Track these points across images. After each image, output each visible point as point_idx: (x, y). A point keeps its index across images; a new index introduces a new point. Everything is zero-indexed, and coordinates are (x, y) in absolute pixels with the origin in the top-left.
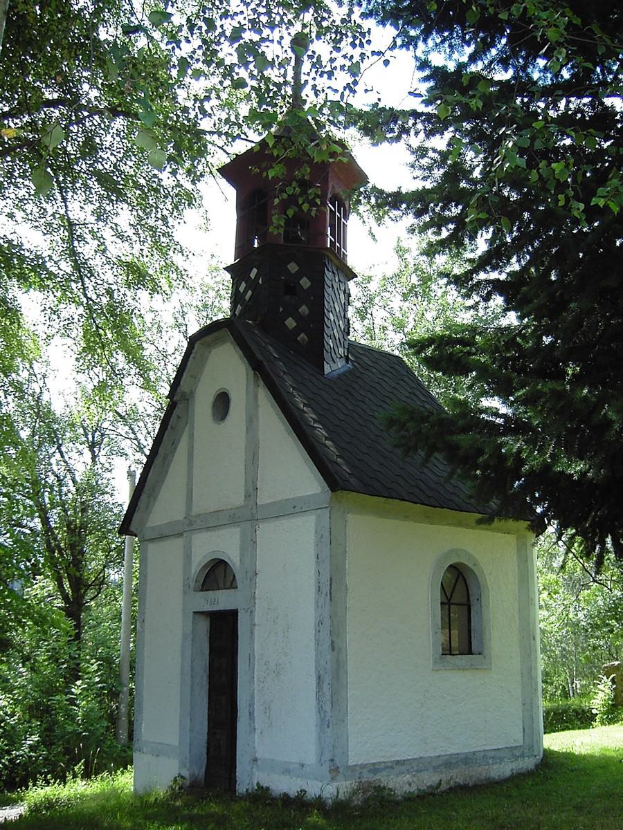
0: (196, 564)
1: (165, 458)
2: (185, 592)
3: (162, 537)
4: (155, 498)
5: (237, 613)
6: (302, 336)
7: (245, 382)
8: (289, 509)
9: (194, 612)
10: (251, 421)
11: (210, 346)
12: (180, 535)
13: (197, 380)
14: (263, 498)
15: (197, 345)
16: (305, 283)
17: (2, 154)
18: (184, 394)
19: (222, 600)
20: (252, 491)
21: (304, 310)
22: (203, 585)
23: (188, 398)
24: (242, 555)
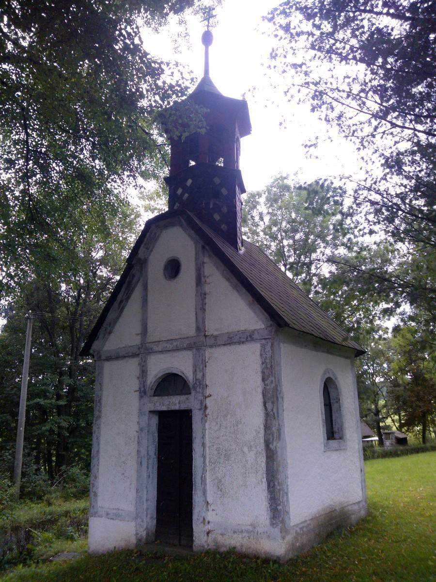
3: (118, 357)
8: (234, 339)
9: (150, 412)
10: (200, 280)
11: (166, 227)
12: (134, 355)
14: (152, 336)
19: (174, 403)
20: (200, 329)
23: (144, 263)
24: (195, 372)
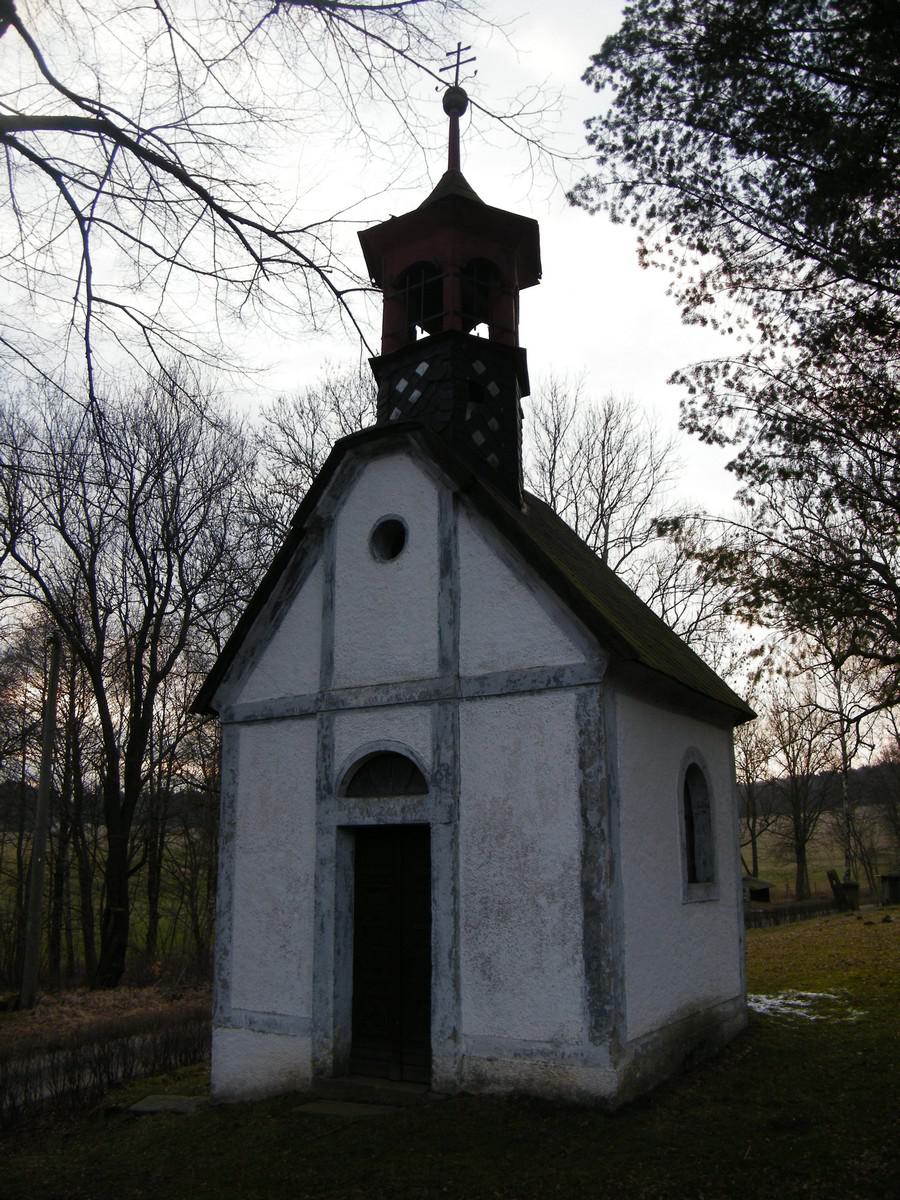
0: (344, 757)
1: (277, 605)
2: (321, 798)
4: (254, 664)
5: (430, 828)
6: (492, 458)
7: (435, 509)
10: (447, 564)
13: (340, 502)
15: (348, 454)
16: (493, 388)
17: (156, 1)
18: (319, 520)
19: (393, 810)
20: (448, 661)
21: (493, 423)
22: (349, 788)
24: (437, 749)
